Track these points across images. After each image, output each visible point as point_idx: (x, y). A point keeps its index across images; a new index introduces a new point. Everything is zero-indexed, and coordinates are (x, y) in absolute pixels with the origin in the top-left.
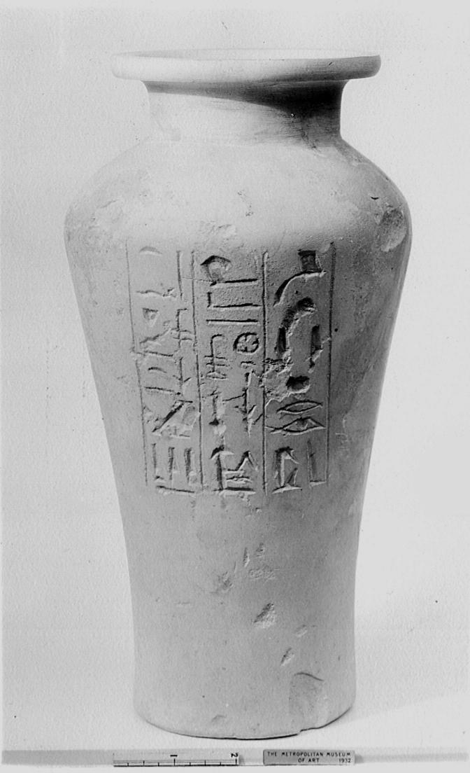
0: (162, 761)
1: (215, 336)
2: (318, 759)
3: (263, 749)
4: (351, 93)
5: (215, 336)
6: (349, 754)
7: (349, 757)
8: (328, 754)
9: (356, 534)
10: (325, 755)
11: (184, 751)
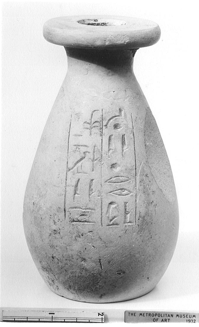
0: (68, 318)
1: (95, 111)
2: (169, 319)
3: (125, 311)
4: (141, 59)
5: (95, 111)
6: (194, 316)
7: (194, 318)
8: (177, 315)
9: (171, 173)
10: (175, 316)
11: (59, 310)
